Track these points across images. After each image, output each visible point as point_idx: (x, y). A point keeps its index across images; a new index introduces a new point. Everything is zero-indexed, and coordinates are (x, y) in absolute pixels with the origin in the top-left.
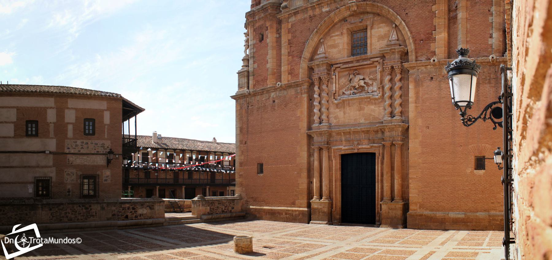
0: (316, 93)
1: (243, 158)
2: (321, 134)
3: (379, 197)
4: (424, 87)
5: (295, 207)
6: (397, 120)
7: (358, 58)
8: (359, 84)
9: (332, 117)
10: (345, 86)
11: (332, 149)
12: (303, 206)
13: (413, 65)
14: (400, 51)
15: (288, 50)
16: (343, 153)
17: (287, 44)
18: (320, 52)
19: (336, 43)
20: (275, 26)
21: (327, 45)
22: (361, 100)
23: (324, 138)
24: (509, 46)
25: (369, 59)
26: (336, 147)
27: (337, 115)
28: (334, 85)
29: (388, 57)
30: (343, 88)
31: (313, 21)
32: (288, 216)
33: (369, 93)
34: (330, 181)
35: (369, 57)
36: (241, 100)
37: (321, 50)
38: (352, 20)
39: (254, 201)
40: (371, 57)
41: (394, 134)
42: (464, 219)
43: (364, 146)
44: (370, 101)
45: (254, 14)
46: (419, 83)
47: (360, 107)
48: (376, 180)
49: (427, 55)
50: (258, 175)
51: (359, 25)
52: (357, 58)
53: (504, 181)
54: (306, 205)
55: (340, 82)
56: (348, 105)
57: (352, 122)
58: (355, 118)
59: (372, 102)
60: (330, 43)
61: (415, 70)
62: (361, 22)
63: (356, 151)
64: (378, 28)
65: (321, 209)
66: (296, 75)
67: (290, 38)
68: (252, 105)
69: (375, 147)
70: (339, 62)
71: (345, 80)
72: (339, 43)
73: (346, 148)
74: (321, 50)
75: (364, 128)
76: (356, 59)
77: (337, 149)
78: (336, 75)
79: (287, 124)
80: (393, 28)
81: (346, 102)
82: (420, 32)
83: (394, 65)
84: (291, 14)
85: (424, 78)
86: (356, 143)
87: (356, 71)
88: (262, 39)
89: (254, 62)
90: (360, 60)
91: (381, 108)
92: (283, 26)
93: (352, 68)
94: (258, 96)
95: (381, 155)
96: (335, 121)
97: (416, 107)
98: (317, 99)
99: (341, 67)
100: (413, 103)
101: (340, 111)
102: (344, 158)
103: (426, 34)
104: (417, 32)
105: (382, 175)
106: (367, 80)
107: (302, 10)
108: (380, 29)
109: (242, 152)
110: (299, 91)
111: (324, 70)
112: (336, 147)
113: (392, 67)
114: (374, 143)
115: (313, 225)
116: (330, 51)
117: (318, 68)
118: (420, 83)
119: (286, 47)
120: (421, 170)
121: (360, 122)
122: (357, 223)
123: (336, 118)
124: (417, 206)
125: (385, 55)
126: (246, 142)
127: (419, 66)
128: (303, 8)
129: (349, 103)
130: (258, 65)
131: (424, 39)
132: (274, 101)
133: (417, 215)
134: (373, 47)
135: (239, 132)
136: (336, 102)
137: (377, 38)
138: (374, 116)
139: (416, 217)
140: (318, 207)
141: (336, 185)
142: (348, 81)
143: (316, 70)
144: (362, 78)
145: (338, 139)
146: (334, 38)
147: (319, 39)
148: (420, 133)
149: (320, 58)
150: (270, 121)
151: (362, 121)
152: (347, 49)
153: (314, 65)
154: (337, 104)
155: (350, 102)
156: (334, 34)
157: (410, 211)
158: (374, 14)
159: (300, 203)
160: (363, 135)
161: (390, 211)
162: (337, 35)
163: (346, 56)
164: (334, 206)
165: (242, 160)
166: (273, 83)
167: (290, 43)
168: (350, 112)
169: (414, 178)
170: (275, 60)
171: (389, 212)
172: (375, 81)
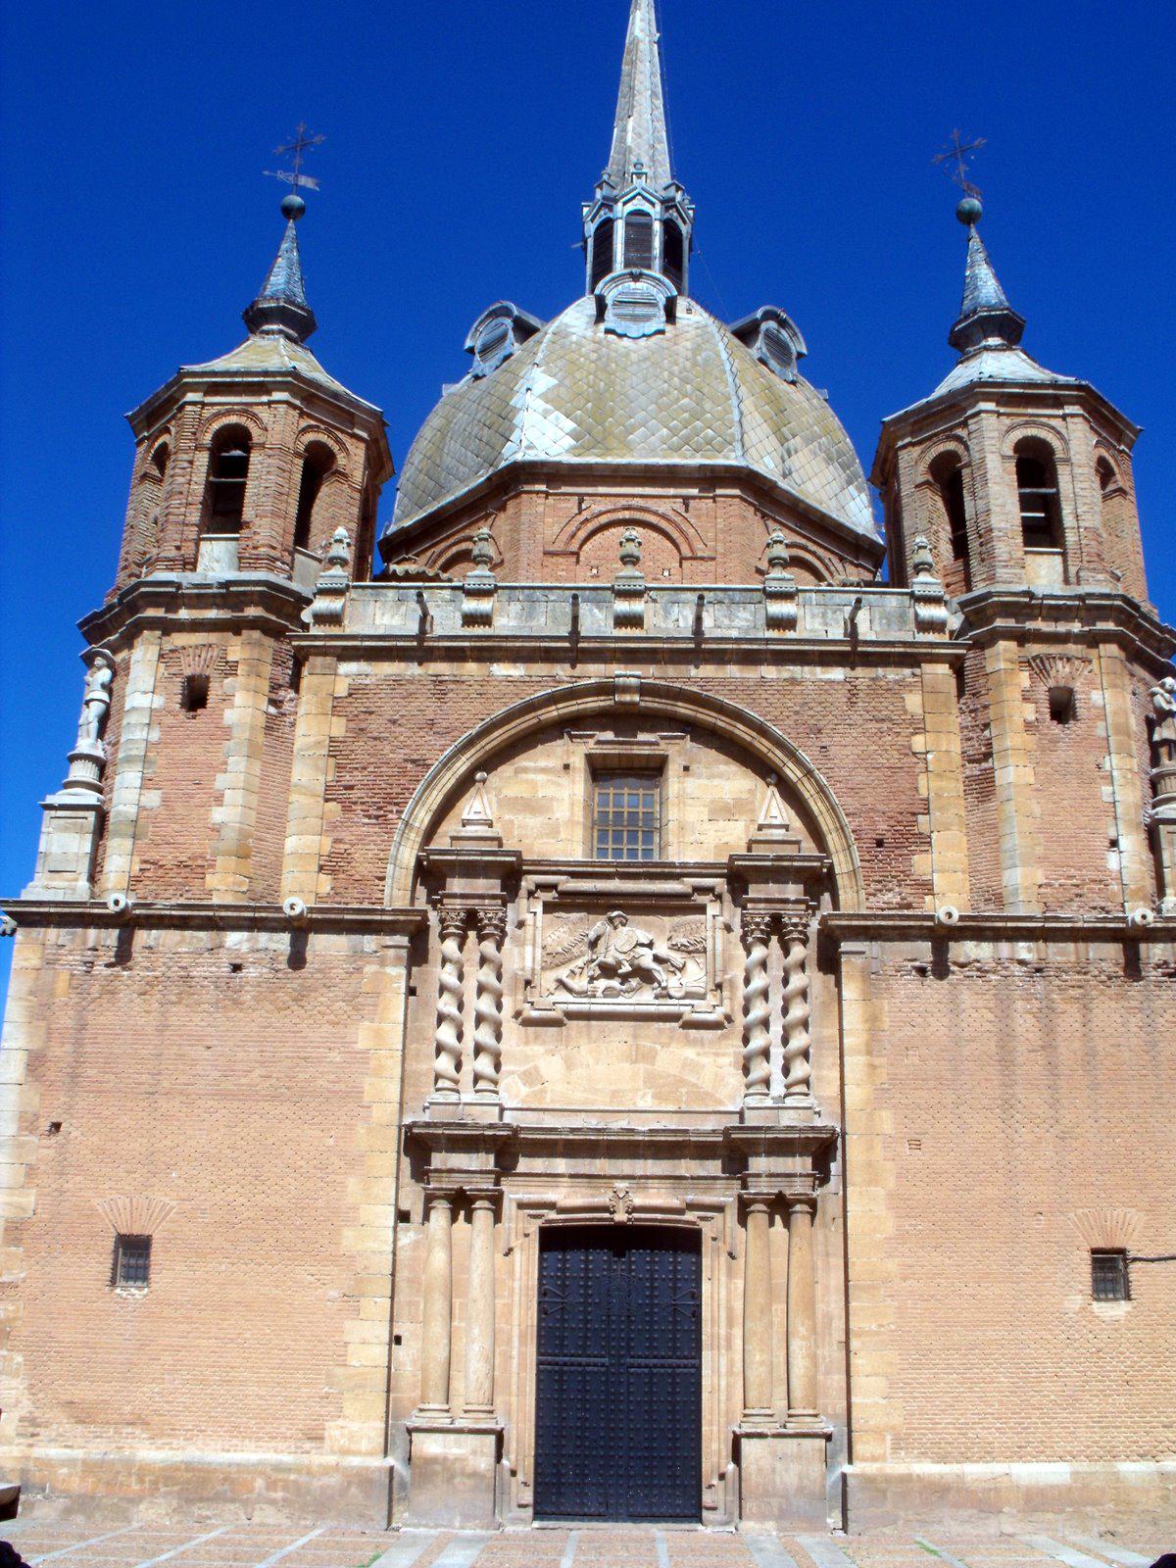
12: (364, 1446)
19: (540, 795)
21: (502, 796)
24: (31, 1464)
27: (536, 1068)
33: (671, 997)
42: (1069, 1489)
53: (406, 1483)
58: (613, 1088)
97: (873, 1067)
100: (859, 1053)
106: (662, 949)
108: (716, 781)
109: (31, 1171)
116: (512, 821)
120: (896, 1304)
123: (530, 1077)
124: (884, 1440)
140: (447, 1451)
146: (531, 776)
148: (889, 1165)
151: (646, 1102)
159: (346, 1431)
161: (779, 1465)
162: (544, 770)
169: (870, 1333)
171: (774, 1470)
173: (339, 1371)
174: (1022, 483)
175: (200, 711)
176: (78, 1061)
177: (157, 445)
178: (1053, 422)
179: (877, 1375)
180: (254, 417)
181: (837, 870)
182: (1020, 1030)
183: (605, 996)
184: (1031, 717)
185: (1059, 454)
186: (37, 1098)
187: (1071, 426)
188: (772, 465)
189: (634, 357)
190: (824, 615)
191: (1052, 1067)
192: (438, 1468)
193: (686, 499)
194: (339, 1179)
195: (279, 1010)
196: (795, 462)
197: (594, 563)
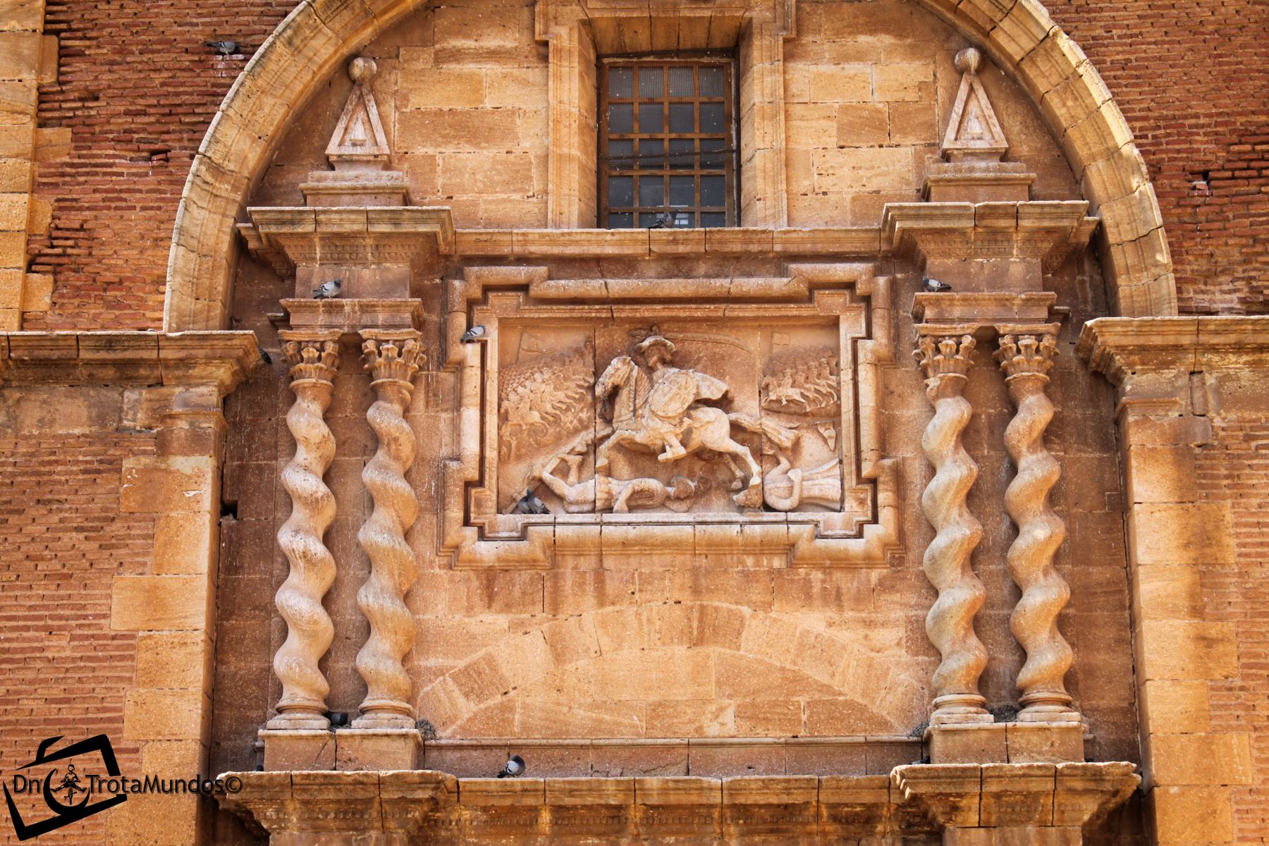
0: (302, 455)
4: (1255, 501)
6: (1055, 738)
7: (685, 242)
9: (441, 672)
10: (558, 440)
13: (1171, 340)
14: (1049, 231)
15: (40, 72)
18: (347, 150)
19: (488, 104)
25: (783, 261)
27: (490, 660)
28: (471, 415)
29: (949, 262)
30: (540, 447)
33: (768, 508)
35: (778, 248)
40: (793, 248)
46: (1212, 467)
47: (702, 607)
49: (1254, 278)
51: (686, 13)
52: (675, 242)
55: (512, 396)
56: (590, 588)
58: (654, 697)
59: (807, 583)
61: (1169, 374)
70: (518, 249)
71: (561, 395)
72: (513, 113)
74: (359, 132)
75: (766, 785)
76: (671, 249)
78: (484, 346)
80: (962, 71)
81: (570, 562)
82: (1185, 117)
83: (1002, 328)
85: (1248, 438)
90: (697, 257)
91: (890, 636)
93: (626, 312)
96: (467, 708)
97: (1205, 641)
98: (313, 504)
100: (1173, 612)
101: (519, 627)
103: (1235, 138)
104: (1165, 118)
106: (749, 411)
108: (852, 68)
110: (137, 419)
111: (389, 288)
113: (988, 341)
117: (339, 262)
118: (1224, 472)
119: (28, 47)
121: (699, 730)
125: (927, 247)
127: (1214, 349)
129: (600, 575)
131: (1223, 169)
134: (803, 184)
136: (487, 551)
137: (834, 125)
138: (827, 689)
142: (581, 399)
144: (717, 396)
146: (469, 67)
147: (345, 51)
149: (354, 192)
152: (583, 168)
153: (304, 236)
154: (490, 568)
155: (609, 563)
156: (470, 44)
162: (494, 55)
163: (575, 218)
168: (605, 642)
172: (814, 428)
181: (1112, 237)
183: (631, 509)
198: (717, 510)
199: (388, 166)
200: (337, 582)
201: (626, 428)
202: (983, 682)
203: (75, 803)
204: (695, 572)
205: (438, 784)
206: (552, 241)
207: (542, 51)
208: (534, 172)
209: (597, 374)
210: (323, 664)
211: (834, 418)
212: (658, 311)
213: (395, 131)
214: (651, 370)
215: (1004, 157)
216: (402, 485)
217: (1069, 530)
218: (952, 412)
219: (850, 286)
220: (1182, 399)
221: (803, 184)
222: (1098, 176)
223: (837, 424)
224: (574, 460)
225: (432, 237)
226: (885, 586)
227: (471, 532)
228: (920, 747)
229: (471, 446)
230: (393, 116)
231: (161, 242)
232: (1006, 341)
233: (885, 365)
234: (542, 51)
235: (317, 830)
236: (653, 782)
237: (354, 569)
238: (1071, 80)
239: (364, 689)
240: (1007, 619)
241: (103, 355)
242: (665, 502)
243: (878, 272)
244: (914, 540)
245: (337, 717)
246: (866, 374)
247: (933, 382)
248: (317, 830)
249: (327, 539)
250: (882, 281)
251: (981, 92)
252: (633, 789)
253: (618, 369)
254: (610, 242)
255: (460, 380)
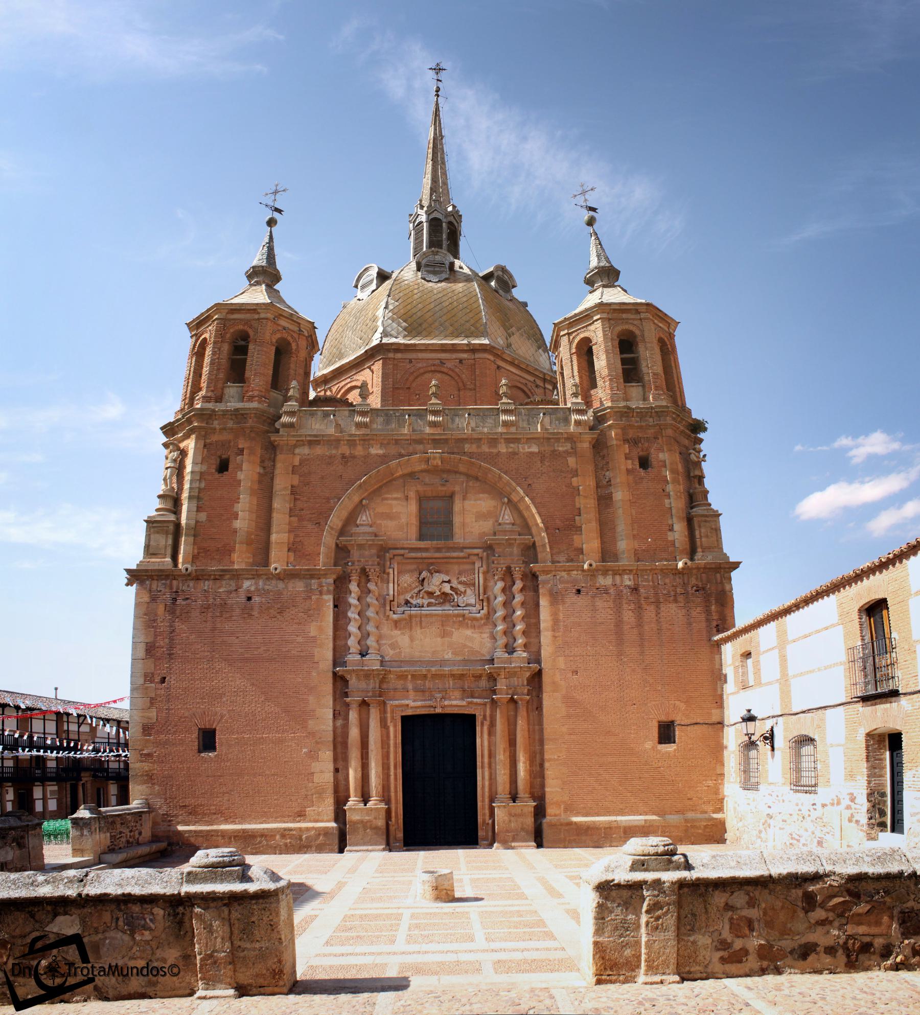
0: (353, 595)
1: (153, 714)
2: (368, 675)
3: (487, 794)
5: (304, 821)
8: (441, 589)
9: (385, 644)
11: (388, 706)
12: (325, 818)
15: (290, 504)
16: (409, 712)
17: (289, 492)
18: (362, 523)
19: (394, 511)
20: (259, 451)
22: (445, 620)
23: (373, 684)
25: (462, 549)
26: (396, 702)
27: (397, 642)
28: (391, 585)
30: (407, 592)
31: (349, 464)
32: (290, 843)
33: (459, 606)
34: (385, 767)
36: (155, 582)
37: (363, 519)
38: (427, 479)
39: (190, 813)
41: (516, 683)
42: (643, 827)
43: (454, 703)
44: (464, 621)
45: (211, 415)
48: (479, 764)
50: (203, 755)
54: (332, 815)
57: (428, 657)
58: (433, 650)
60: (381, 509)
62: (443, 485)
63: (439, 710)
64: (475, 500)
65: (370, 821)
66: (307, 555)
67: (296, 482)
68: (187, 599)
69: (476, 704)
73: (419, 703)
74: (364, 518)
75: (458, 670)
77: (397, 706)
79: (284, 650)
80: (503, 503)
83: (512, 566)
84: (302, 441)
86: (439, 695)
87: (434, 567)
88: (223, 467)
89: (198, 507)
90: (443, 548)
91: (486, 635)
92: (280, 457)
93: (426, 561)
94: (206, 582)
95: (488, 719)
96: (391, 652)
97: (555, 637)
98: (356, 606)
99: (405, 556)
101: (403, 634)
102: (410, 723)
105: (491, 755)
106: (455, 583)
107: (329, 441)
108: (479, 502)
109: (152, 701)
110: (315, 587)
112: (396, 702)
113: (509, 569)
114: (473, 697)
115: (351, 854)
119: (287, 498)
122: (436, 845)
123: (393, 646)
124: (560, 808)
126: (165, 678)
128: (332, 438)
130: (208, 517)
132: (249, 599)
133: (562, 825)
135: (141, 653)
136: (395, 616)
139: (560, 827)
141: (396, 775)
143: (355, 554)
145: (399, 686)
146: (390, 502)
150: (238, 637)
151: (449, 656)
155: (423, 619)
157: (548, 817)
158: (468, 476)
160: (451, 682)
162: (396, 499)
164: (393, 814)
165: (149, 718)
166: (247, 560)
167: (294, 492)
169: (554, 760)
170: (254, 516)
173: (310, 784)
174: (621, 352)
175: (225, 473)
176: (171, 647)
177: (201, 338)
178: (635, 322)
179: (557, 778)
180: (251, 327)
181: (537, 544)
182: (625, 619)
183: (428, 606)
184: (630, 467)
185: (639, 339)
186: (153, 666)
187: (644, 324)
188: (502, 342)
189: (435, 292)
190: (528, 420)
191: (641, 635)
192: (359, 826)
193: (461, 361)
194: (305, 697)
195: (271, 618)
196: (512, 340)
197: (417, 392)
198: (447, 607)
199: (371, 526)
200: (361, 624)
201: (427, 588)
202: (506, 646)
203: (56, 984)
204: (442, 621)
205: (386, 670)
206: (409, 544)
207: (407, 498)
208: (405, 527)
209: (420, 575)
210: (359, 643)
211: (474, 585)
212: (434, 560)
213: (373, 517)
214: (432, 574)
215: (513, 524)
216: (376, 602)
217: (526, 611)
218: (500, 585)
219: (478, 555)
220: (551, 582)
221: (467, 530)
222: (534, 530)
223: (474, 586)
224: (415, 595)
225: (382, 545)
226: (485, 624)
227: (392, 612)
228: (492, 661)
229: (391, 592)
230: (372, 514)
231: (319, 545)
232: (513, 569)
233: (485, 573)
234: (407, 498)
235: (359, 680)
236: (433, 669)
237: (365, 621)
238: (528, 507)
239: (368, 648)
240: (511, 632)
241: (307, 573)
242: (435, 605)
243: (484, 551)
244: (491, 613)
245: (363, 654)
246: (481, 575)
247: (496, 578)
248: (359, 680)
249: (359, 614)
250: (485, 554)
251: (508, 509)
252: (429, 671)
253: (424, 574)
254: (422, 544)
255: (389, 577)
